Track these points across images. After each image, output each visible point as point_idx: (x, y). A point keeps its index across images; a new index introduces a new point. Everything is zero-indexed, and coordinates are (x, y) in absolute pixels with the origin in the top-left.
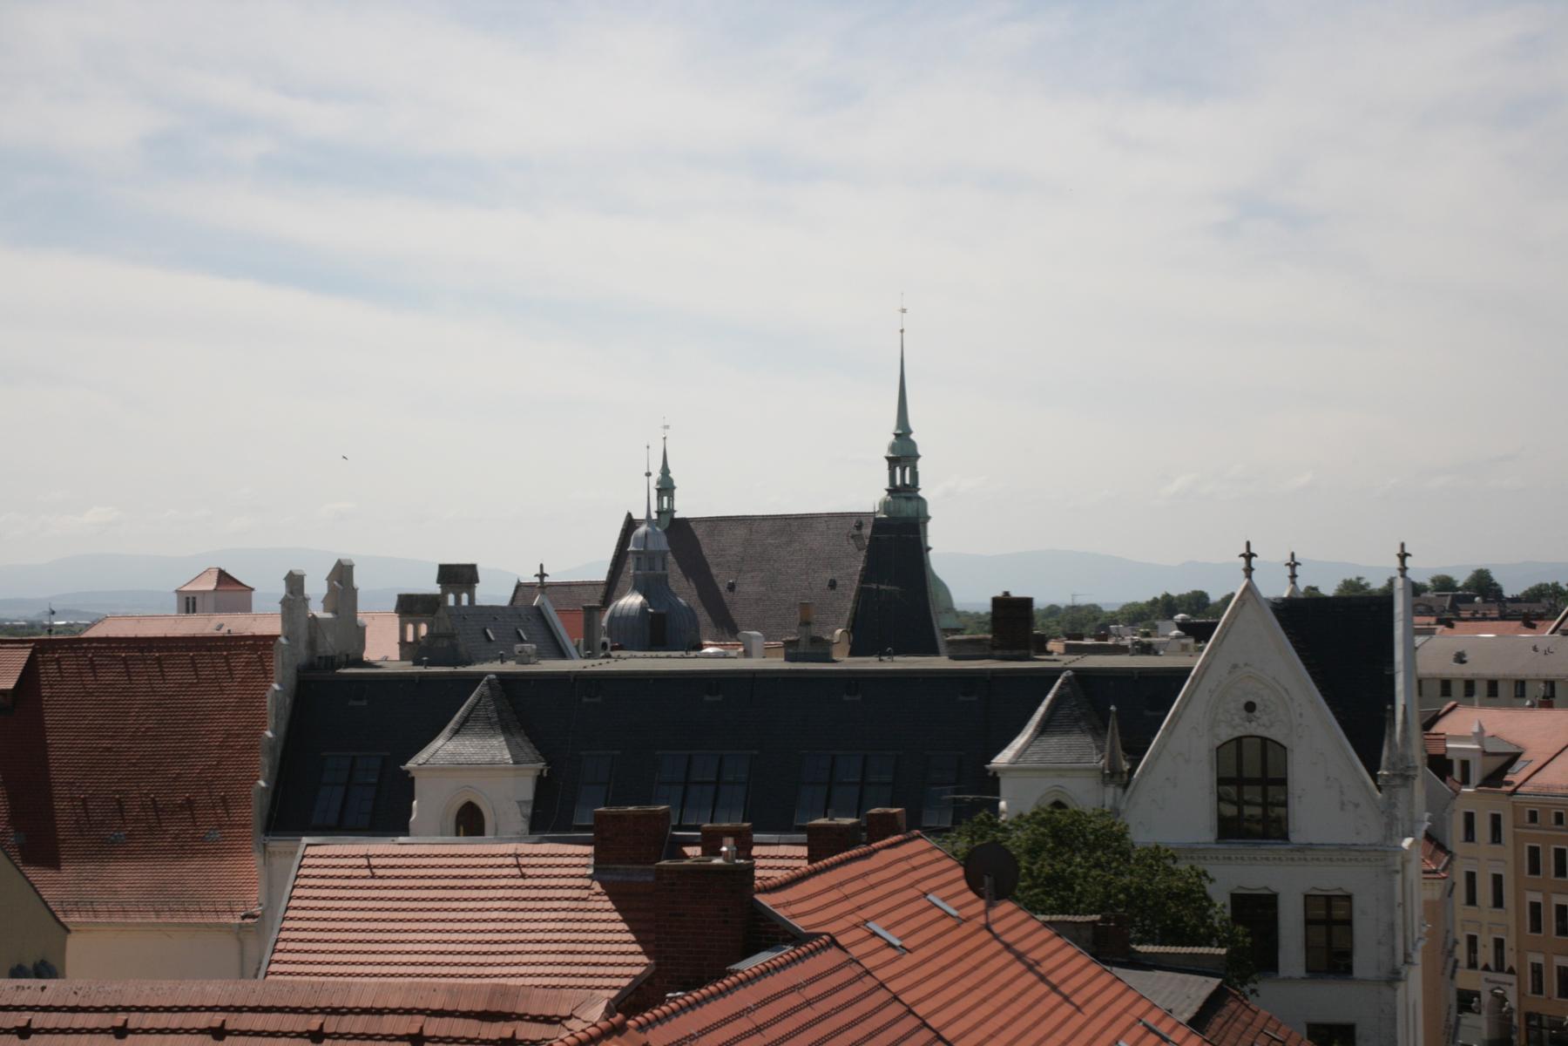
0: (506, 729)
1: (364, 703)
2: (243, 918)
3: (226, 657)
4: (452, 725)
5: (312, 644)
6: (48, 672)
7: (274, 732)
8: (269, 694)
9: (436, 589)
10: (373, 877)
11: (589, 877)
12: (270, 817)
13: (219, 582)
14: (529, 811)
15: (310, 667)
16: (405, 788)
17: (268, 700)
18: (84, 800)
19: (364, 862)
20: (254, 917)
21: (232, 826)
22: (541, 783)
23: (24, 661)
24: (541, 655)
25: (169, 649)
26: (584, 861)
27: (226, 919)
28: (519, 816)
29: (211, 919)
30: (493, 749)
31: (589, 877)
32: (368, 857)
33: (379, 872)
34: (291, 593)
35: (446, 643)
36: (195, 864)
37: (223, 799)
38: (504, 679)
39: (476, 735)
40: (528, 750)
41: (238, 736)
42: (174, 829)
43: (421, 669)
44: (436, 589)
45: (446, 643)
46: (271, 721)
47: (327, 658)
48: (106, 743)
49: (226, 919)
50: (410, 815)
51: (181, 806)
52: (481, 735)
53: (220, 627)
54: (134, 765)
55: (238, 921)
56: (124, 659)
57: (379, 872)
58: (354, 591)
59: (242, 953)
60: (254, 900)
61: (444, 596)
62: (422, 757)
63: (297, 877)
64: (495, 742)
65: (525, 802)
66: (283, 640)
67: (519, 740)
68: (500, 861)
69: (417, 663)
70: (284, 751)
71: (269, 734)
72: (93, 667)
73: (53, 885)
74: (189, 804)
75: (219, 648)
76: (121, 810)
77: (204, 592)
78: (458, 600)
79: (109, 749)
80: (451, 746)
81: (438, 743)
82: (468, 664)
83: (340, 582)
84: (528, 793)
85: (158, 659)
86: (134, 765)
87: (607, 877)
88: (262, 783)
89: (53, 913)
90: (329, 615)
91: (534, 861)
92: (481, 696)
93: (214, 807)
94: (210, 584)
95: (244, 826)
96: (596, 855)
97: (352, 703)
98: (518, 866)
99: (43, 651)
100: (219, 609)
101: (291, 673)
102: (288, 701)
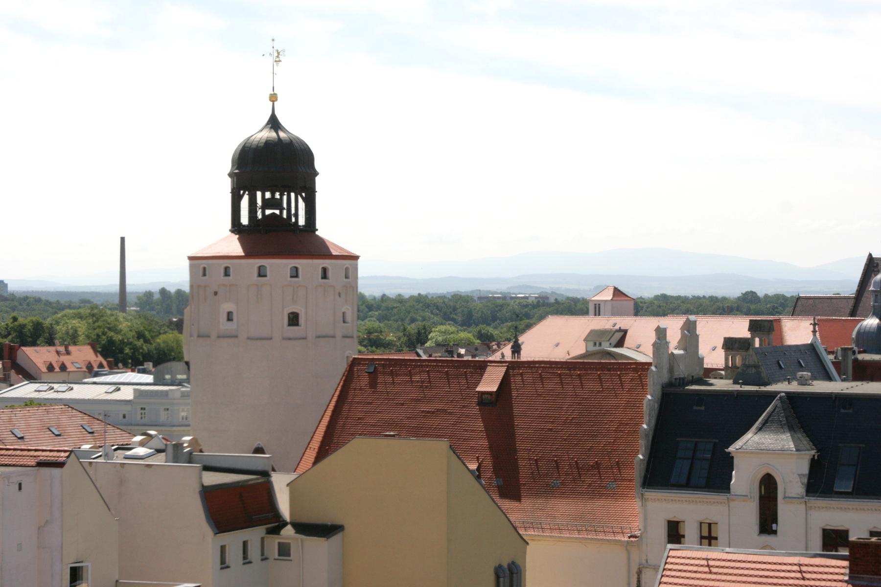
0: (791, 429)
1: (703, 408)
2: (629, 537)
3: (619, 375)
4: (757, 424)
5: (671, 370)
6: (516, 382)
8: (645, 402)
9: (748, 335)
10: (710, 573)
11: (846, 581)
12: (645, 477)
13: (614, 295)
14: (805, 480)
15: (670, 384)
16: (728, 463)
18: (536, 460)
19: (704, 562)
20: (635, 537)
22: (814, 465)
23: (502, 374)
24: (814, 378)
25: (586, 370)
26: (843, 571)
27: (619, 537)
28: (800, 484)
29: (610, 537)
30: (784, 441)
31: (846, 581)
32: (707, 559)
33: (714, 570)
34: (659, 339)
35: (754, 370)
36: (601, 502)
38: (791, 397)
39: (773, 431)
40: (805, 442)
41: (627, 424)
42: (588, 480)
43: (737, 387)
44: (748, 335)
45: (754, 370)
46: (646, 418)
47: (680, 379)
48: (549, 426)
49: (619, 537)
50: (731, 480)
51: (592, 466)
52: (776, 432)
53: (615, 325)
54: (565, 440)
55: (626, 539)
56: (560, 375)
57: (714, 570)
58: (697, 336)
59: (629, 559)
60: (636, 527)
61: (753, 338)
62: (738, 444)
63: (664, 569)
64: (784, 436)
65: (804, 475)
66: (653, 368)
67: (800, 436)
68: (789, 568)
69: (735, 382)
70: (654, 438)
71: (645, 426)
72: (541, 378)
73: (516, 511)
74: (597, 466)
75: (615, 370)
76: (558, 467)
77: (606, 301)
78: (273, 195)
79: (551, 430)
80: (756, 438)
81: (749, 435)
82: (765, 384)
83: (688, 331)
84: (806, 470)
85: (579, 375)
87: (857, 582)
88: (641, 457)
89: (515, 528)
90: (681, 352)
91: (810, 569)
92: (776, 407)
93: (612, 468)
94: (608, 296)
95: (630, 481)
96: (851, 568)
97: (695, 408)
98: (800, 572)
100: (614, 313)
101: (659, 393)
102: (656, 406)
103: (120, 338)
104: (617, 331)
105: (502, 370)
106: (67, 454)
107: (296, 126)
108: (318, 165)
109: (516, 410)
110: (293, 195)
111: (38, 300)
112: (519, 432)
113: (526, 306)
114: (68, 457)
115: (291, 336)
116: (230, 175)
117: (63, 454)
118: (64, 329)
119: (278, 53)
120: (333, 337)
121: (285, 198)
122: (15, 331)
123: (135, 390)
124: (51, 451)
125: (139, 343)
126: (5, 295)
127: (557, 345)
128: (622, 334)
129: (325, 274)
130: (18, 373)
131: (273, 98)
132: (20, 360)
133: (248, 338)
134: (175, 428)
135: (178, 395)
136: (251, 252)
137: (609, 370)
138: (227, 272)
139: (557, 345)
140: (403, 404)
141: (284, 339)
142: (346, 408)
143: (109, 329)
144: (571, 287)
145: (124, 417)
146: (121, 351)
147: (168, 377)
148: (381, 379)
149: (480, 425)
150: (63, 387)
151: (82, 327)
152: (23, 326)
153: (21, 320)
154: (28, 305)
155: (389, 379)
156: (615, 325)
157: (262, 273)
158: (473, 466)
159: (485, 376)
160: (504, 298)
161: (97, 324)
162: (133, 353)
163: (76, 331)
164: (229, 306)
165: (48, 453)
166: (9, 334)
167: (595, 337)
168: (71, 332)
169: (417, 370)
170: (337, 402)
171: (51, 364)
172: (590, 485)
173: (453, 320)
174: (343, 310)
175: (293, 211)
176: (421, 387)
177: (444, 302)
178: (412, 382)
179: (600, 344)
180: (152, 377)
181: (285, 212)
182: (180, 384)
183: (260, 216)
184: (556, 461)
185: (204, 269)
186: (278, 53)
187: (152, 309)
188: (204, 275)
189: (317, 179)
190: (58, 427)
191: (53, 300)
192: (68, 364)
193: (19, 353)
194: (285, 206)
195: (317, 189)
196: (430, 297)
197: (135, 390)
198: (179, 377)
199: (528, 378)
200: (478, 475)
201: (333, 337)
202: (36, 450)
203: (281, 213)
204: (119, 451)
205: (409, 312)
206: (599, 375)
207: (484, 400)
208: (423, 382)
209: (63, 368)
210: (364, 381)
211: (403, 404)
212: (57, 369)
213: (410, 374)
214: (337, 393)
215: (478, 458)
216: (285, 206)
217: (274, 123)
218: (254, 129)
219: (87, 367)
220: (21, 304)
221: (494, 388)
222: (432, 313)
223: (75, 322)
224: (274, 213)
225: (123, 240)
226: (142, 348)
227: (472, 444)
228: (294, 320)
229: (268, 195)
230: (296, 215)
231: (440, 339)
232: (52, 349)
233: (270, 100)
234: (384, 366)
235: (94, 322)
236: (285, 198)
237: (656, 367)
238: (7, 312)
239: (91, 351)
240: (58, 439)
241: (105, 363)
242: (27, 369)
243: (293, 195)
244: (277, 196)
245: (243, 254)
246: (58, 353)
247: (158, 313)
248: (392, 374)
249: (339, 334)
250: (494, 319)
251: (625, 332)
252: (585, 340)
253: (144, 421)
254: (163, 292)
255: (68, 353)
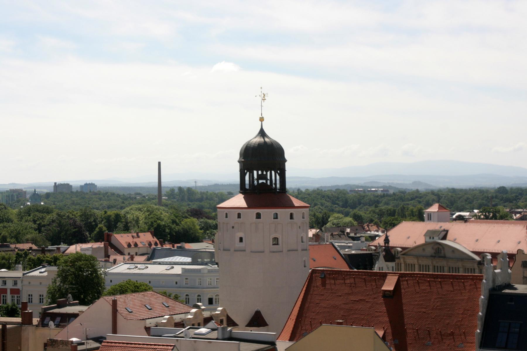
1: (513, 303)
5: (494, 281)
6: (404, 285)
7: (482, 313)
8: (480, 300)
12: (481, 342)
13: (439, 208)
17: (480, 302)
18: (417, 330)
21: (468, 343)
23: (396, 280)
25: (444, 278)
37: (464, 333)
41: (468, 310)
48: (424, 310)
51: (450, 334)
53: (441, 227)
54: (433, 318)
56: (429, 281)
71: (480, 314)
72: (418, 283)
74: (452, 334)
75: (461, 279)
76: (429, 334)
78: (262, 172)
79: (425, 312)
85: (440, 281)
86: (433, 318)
88: (478, 331)
93: (461, 335)
95: (472, 343)
97: (509, 303)
99: (402, 277)
100: (440, 220)
101: (487, 293)
102: (486, 302)
103: (164, 223)
104: (442, 231)
105: (396, 278)
106: (172, 348)
107: (275, 135)
108: (286, 156)
109: (404, 301)
110: (273, 172)
111: (113, 194)
112: (406, 313)
113: (377, 196)
114: (172, 349)
115: (275, 250)
116: (239, 162)
117: (170, 347)
118: (132, 217)
119: (264, 95)
120: (297, 250)
121: (269, 173)
122: (105, 219)
123: (183, 269)
124: (163, 345)
125: (173, 226)
126: (96, 191)
127: (409, 238)
128: (445, 233)
129: (291, 217)
130: (112, 248)
131: (262, 119)
132: (113, 241)
133: (251, 252)
134: (204, 290)
135: (206, 271)
136: (251, 205)
137: (457, 279)
138: (239, 216)
139: (409, 238)
140: (340, 296)
141: (270, 252)
142: (309, 297)
143: (157, 218)
144: (399, 182)
145: (176, 283)
146: (164, 231)
147: (199, 260)
148: (328, 281)
149: (384, 308)
150: (143, 266)
151: (142, 216)
152: (110, 216)
153: (109, 213)
154: (108, 197)
155: (333, 282)
156: (441, 227)
157: (258, 216)
158: (381, 333)
159: (386, 281)
160: (364, 191)
161: (150, 216)
162: (170, 231)
163: (138, 218)
164: (241, 235)
165: (161, 347)
166: (102, 221)
167: (430, 234)
168: (135, 218)
169: (348, 277)
170: (305, 294)
171: (129, 243)
172: (449, 345)
173: (338, 204)
174: (302, 235)
175: (274, 182)
176: (351, 286)
177: (332, 195)
178: (345, 283)
179: (433, 238)
180: (190, 258)
181: (269, 182)
182: (206, 264)
183: (256, 182)
184: (428, 331)
185: (227, 214)
186: (264, 95)
187: (174, 198)
188: (227, 217)
189: (286, 164)
190: (150, 305)
191: (121, 193)
192: (139, 243)
193: (112, 238)
194: (269, 178)
195: (286, 169)
196: (323, 190)
197: (183, 269)
198: (205, 260)
199: (411, 282)
200: (384, 338)
201: (297, 250)
202: (155, 345)
203: (267, 182)
204: (191, 330)
205: (313, 200)
206: (452, 282)
207: (386, 295)
208: (351, 284)
209: (136, 245)
210: (319, 282)
211: (340, 296)
212: (133, 246)
213: (344, 279)
214: (305, 289)
215: (384, 327)
216: (269, 178)
217: (262, 133)
218: (250, 136)
219: (149, 245)
220: (104, 197)
221: (392, 288)
222: (326, 200)
223: (137, 213)
224: (263, 183)
225: (159, 163)
226: (175, 228)
227: (381, 319)
228: (276, 241)
229: (260, 172)
230: (276, 184)
231: (335, 221)
232: (130, 235)
233: (260, 120)
234: (329, 274)
235: (149, 215)
236: (269, 173)
237: (486, 280)
238: (97, 201)
239: (151, 235)
240: (151, 311)
241: (158, 242)
242: (120, 249)
243: (273, 172)
244: (265, 173)
245: (246, 206)
246: (133, 237)
247: (178, 201)
248: (334, 279)
249: (300, 249)
250: (360, 204)
251: (447, 231)
252: (425, 235)
253: (187, 286)
254: (180, 189)
255: (138, 237)
